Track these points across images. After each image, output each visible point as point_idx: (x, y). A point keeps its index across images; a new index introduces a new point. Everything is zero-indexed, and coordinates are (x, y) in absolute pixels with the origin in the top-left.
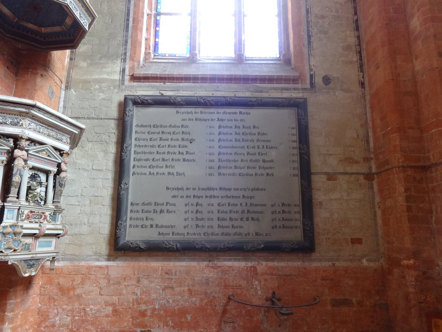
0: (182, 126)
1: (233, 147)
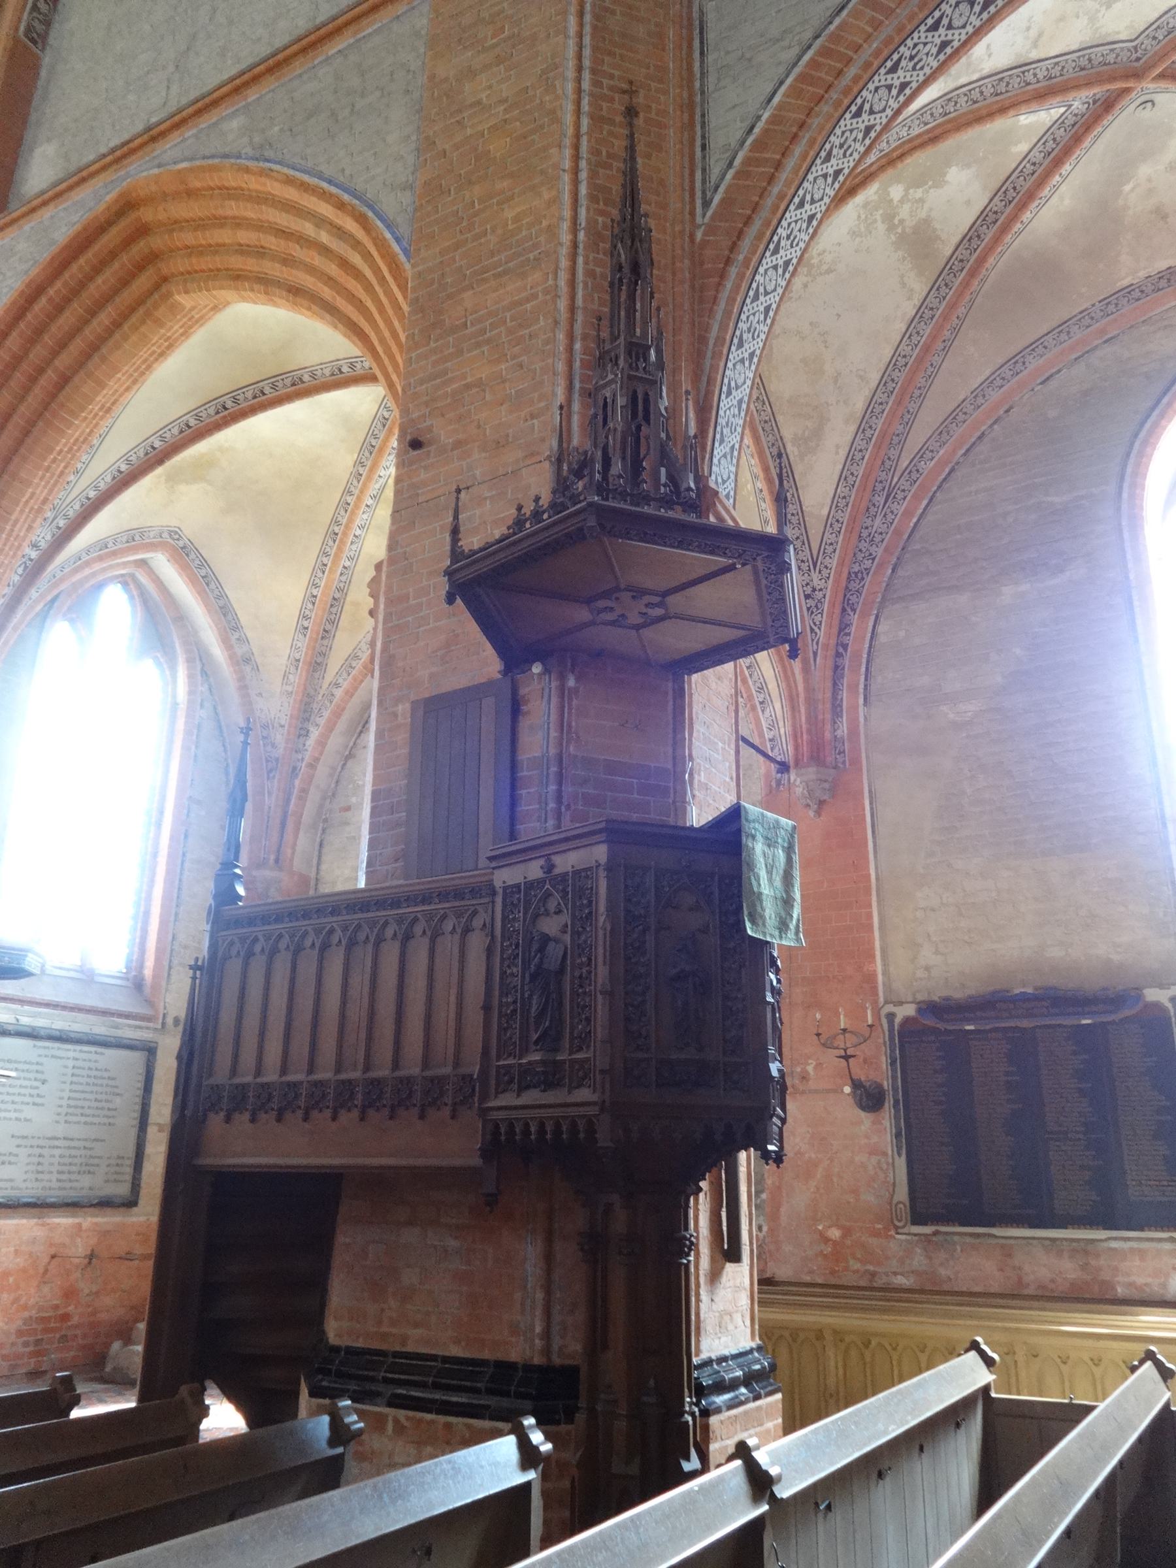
0: (37, 1063)
1: (83, 1092)
